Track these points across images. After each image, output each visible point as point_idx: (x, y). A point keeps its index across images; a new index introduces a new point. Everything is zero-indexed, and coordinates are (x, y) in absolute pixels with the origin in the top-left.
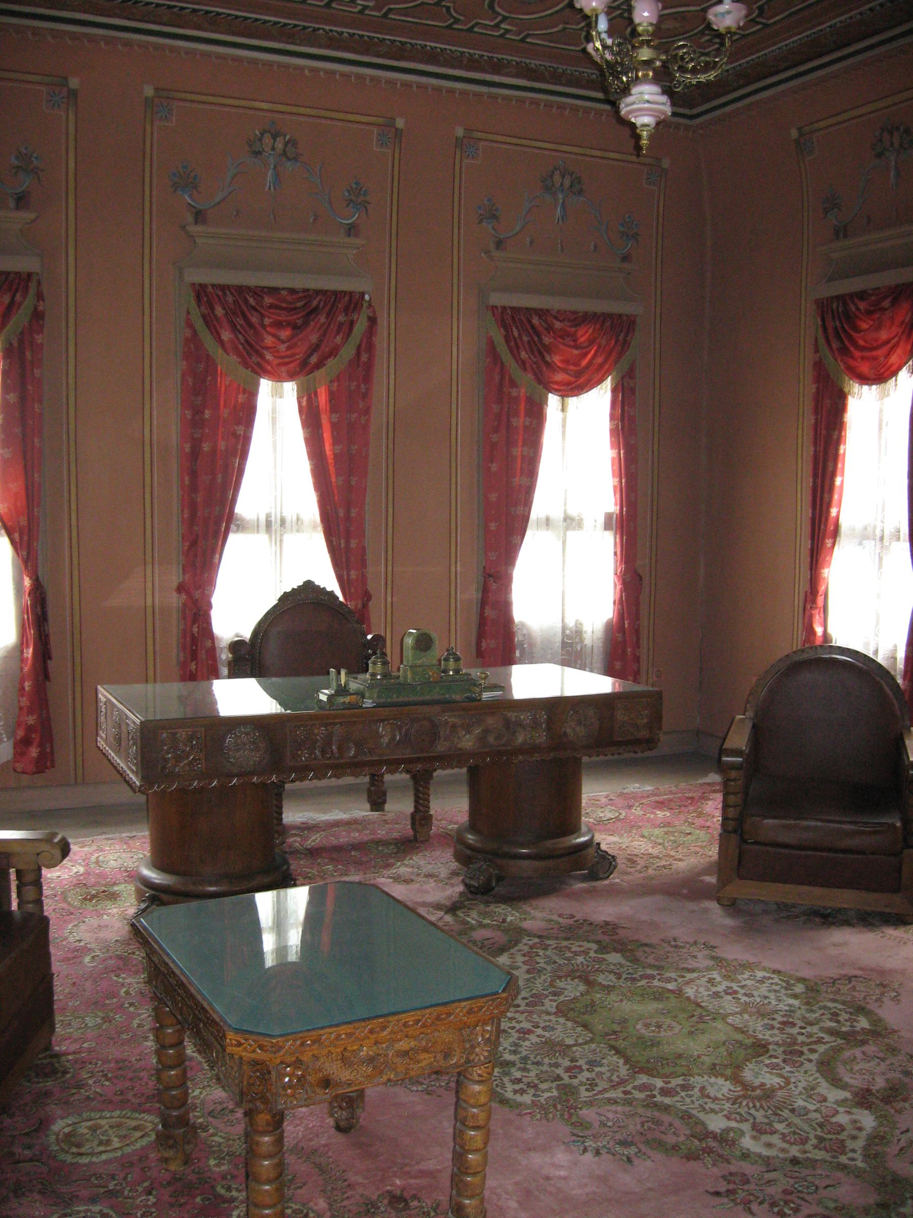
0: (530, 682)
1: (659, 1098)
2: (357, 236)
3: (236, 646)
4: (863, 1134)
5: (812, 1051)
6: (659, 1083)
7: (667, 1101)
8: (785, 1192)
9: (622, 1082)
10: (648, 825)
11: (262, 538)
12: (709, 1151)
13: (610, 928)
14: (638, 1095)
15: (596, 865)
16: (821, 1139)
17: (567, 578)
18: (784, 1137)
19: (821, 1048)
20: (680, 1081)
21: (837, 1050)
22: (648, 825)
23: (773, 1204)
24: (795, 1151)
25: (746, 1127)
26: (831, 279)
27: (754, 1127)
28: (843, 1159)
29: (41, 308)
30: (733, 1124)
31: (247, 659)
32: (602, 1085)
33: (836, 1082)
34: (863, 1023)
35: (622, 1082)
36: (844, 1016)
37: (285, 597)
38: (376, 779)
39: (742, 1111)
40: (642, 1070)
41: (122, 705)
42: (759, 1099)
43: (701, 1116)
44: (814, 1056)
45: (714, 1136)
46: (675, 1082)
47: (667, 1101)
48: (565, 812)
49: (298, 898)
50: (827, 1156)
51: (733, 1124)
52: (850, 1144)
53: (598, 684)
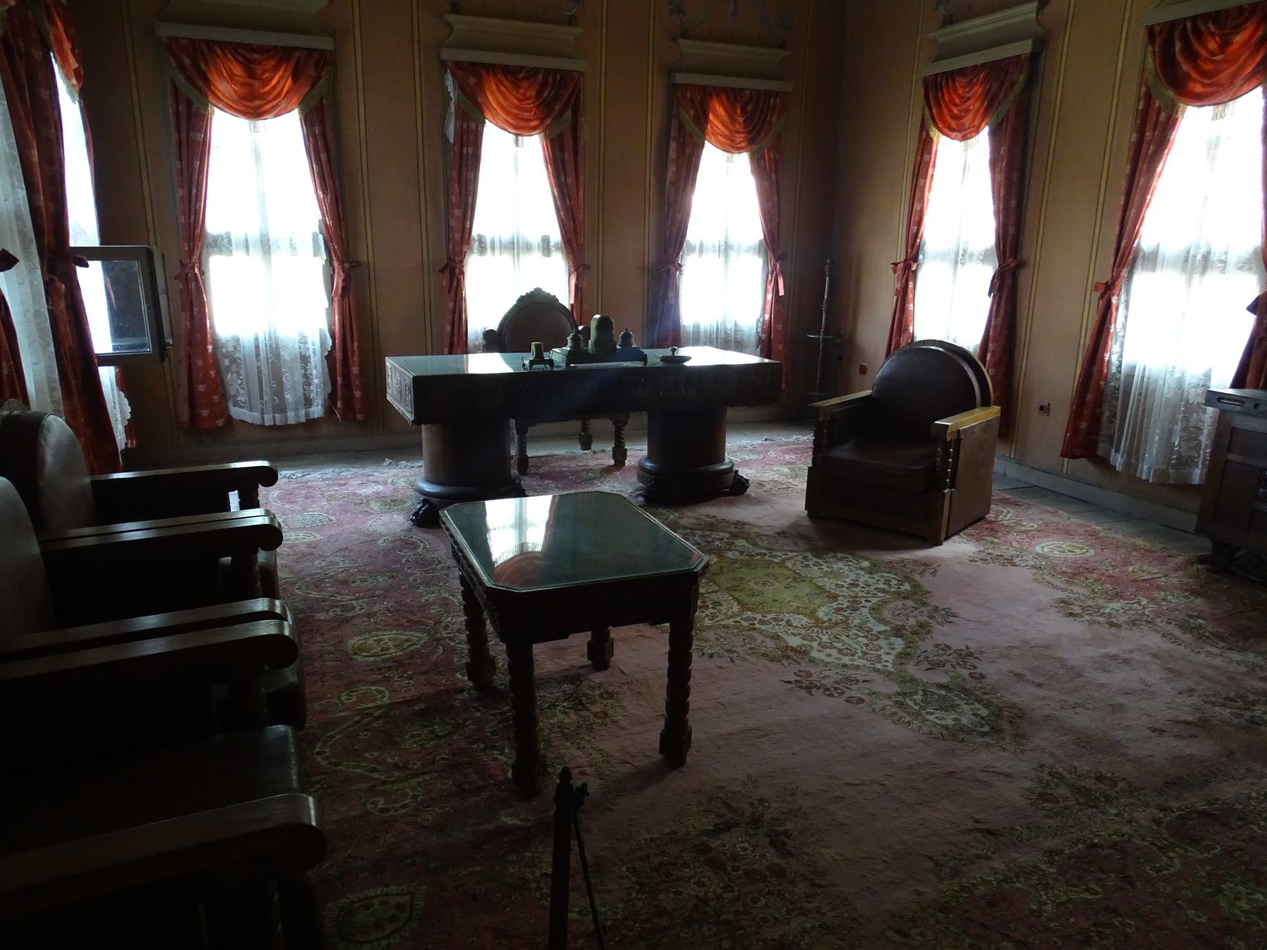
0: (699, 357)
1: (757, 626)
2: (576, 26)
3: (488, 334)
4: (895, 652)
5: (868, 601)
6: (759, 616)
7: (763, 627)
8: (836, 682)
9: (734, 615)
10: (771, 464)
11: (507, 257)
12: (788, 657)
13: (738, 524)
14: (745, 624)
15: (738, 487)
16: (865, 653)
17: (724, 288)
18: (840, 651)
19: (874, 600)
20: (773, 616)
21: (885, 602)
22: (771, 464)
23: (827, 689)
24: (846, 660)
25: (815, 644)
26: (936, 60)
27: (820, 644)
28: (878, 666)
29: (481, 341)
30: (805, 642)
31: (493, 342)
32: (720, 617)
33: (882, 621)
34: (907, 587)
35: (734, 615)
36: (894, 582)
37: (522, 300)
38: (585, 427)
39: (814, 635)
40: (748, 609)
41: (398, 373)
42: (829, 627)
43: (785, 636)
44: (868, 605)
45: (792, 649)
46: (769, 617)
47: (763, 627)
48: (715, 451)
49: (538, 508)
50: (868, 664)
51: (805, 642)
52: (885, 657)
53: (754, 359)
